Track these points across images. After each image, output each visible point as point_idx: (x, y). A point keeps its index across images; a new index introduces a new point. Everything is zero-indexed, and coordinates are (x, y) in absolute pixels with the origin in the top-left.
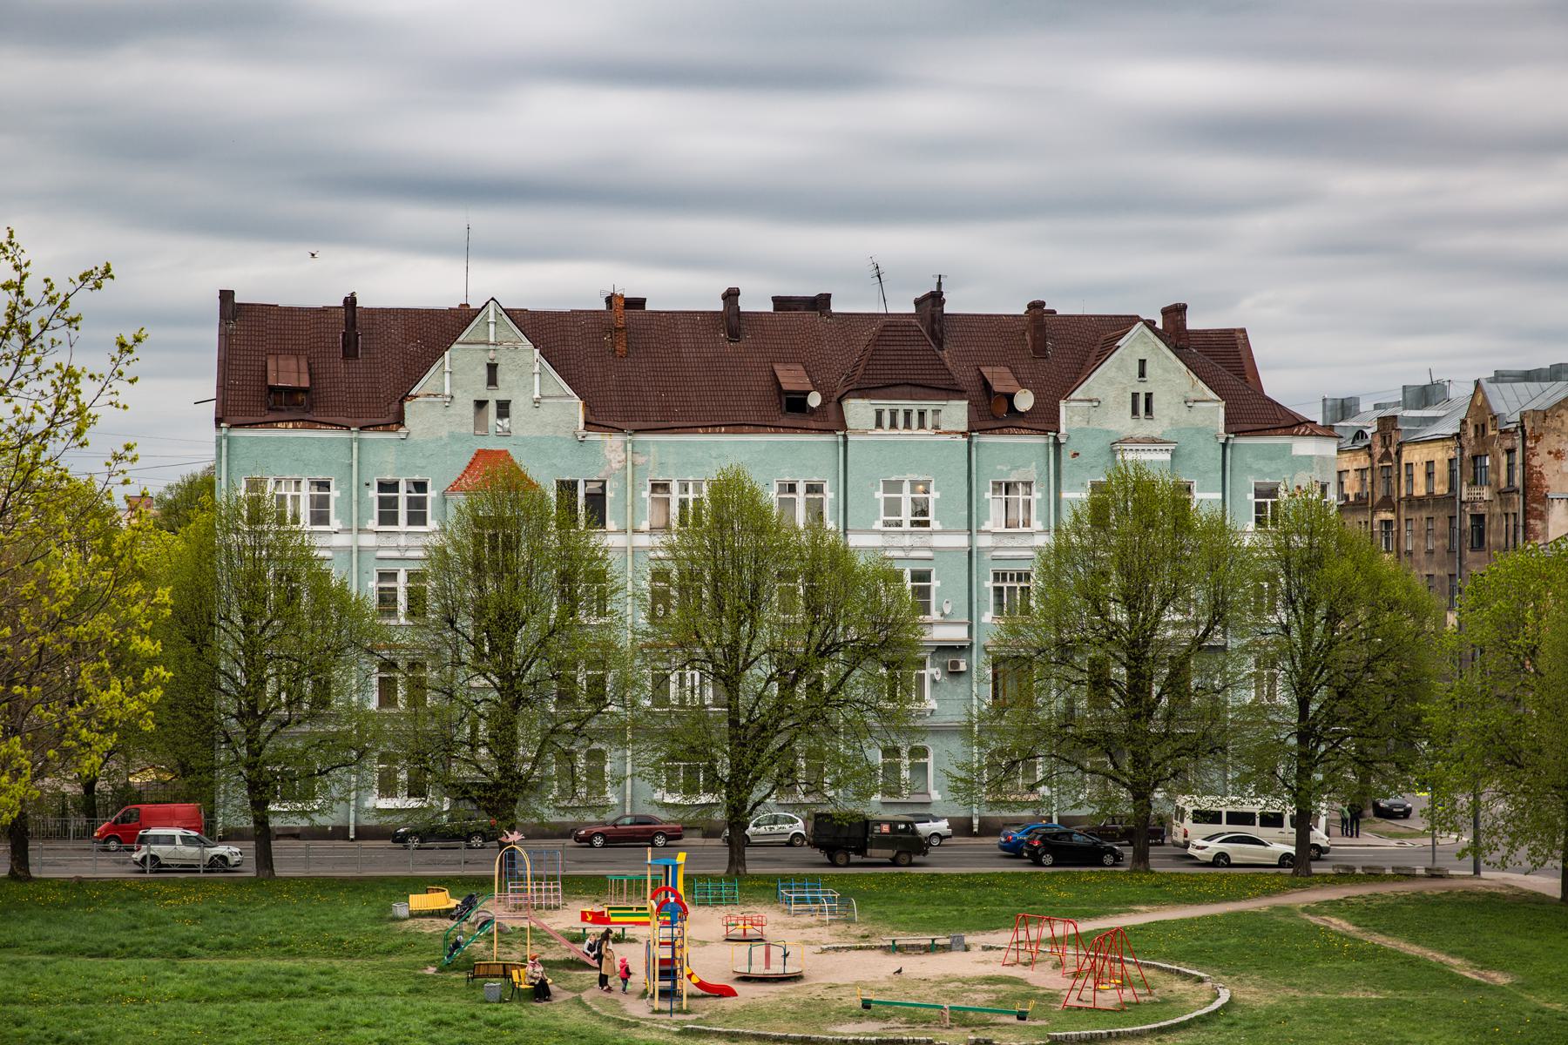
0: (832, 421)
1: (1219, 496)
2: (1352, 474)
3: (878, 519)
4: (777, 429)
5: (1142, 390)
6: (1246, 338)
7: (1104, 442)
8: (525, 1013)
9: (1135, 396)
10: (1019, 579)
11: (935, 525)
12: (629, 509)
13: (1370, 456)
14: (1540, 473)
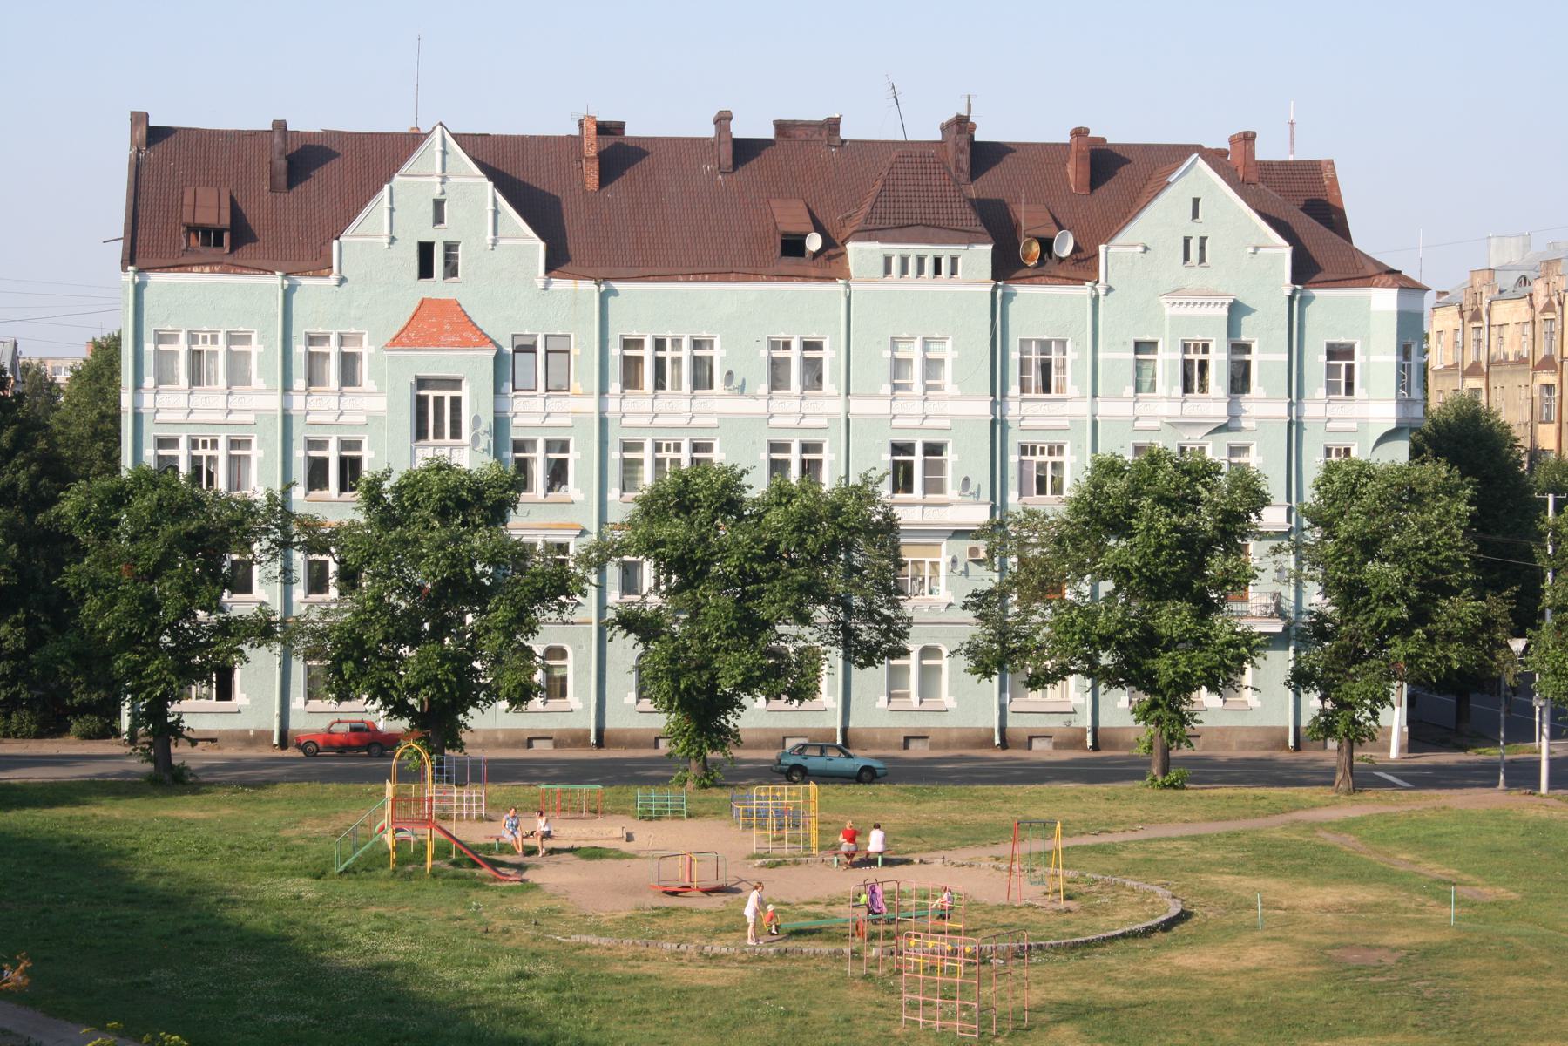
0: (830, 263)
2: (1512, 326)
4: (771, 277)
5: (1195, 233)
6: (1333, 170)
10: (1051, 453)
11: (950, 388)
13: (1532, 306)
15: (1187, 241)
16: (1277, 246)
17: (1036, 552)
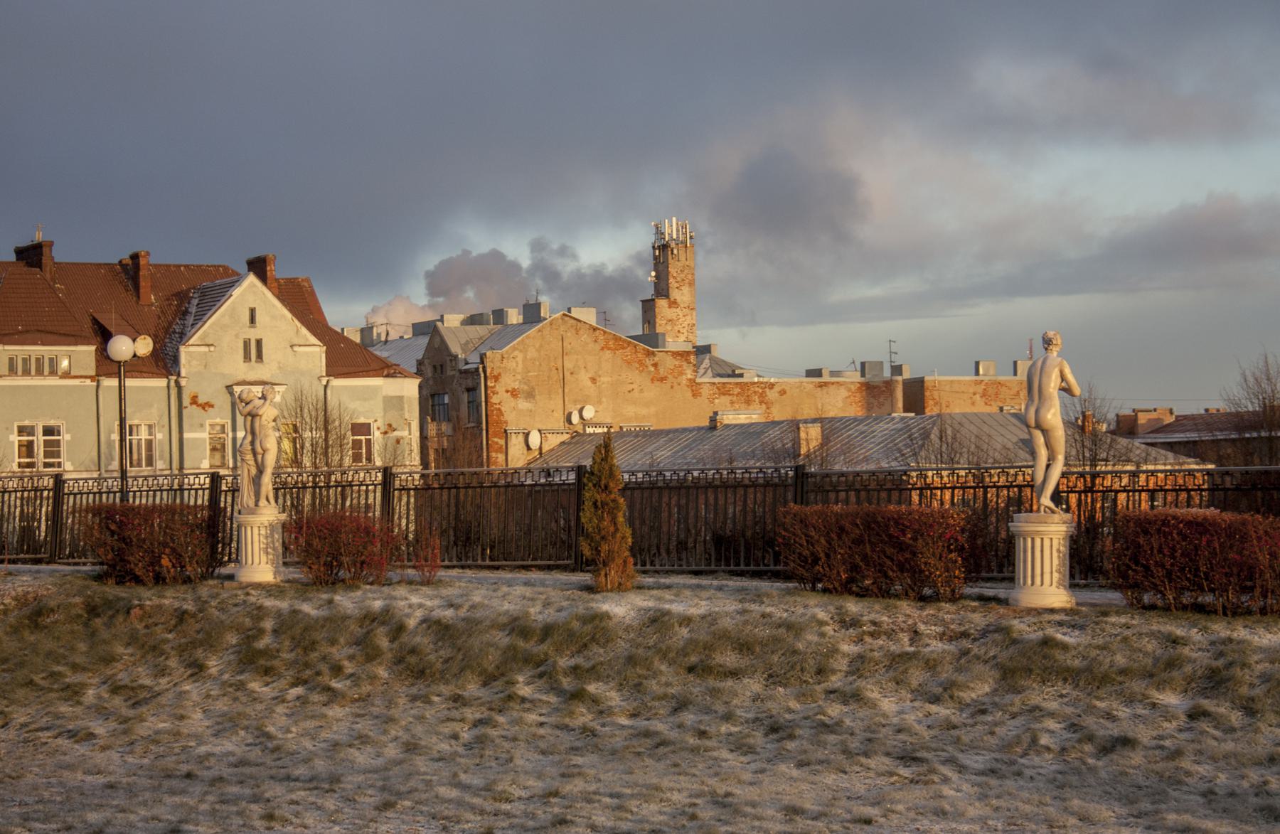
1: (186, 435)
3: (13, 461)
5: (253, 335)
7: (220, 386)
8: (332, 767)
9: (247, 344)
12: (484, 432)
14: (499, 409)
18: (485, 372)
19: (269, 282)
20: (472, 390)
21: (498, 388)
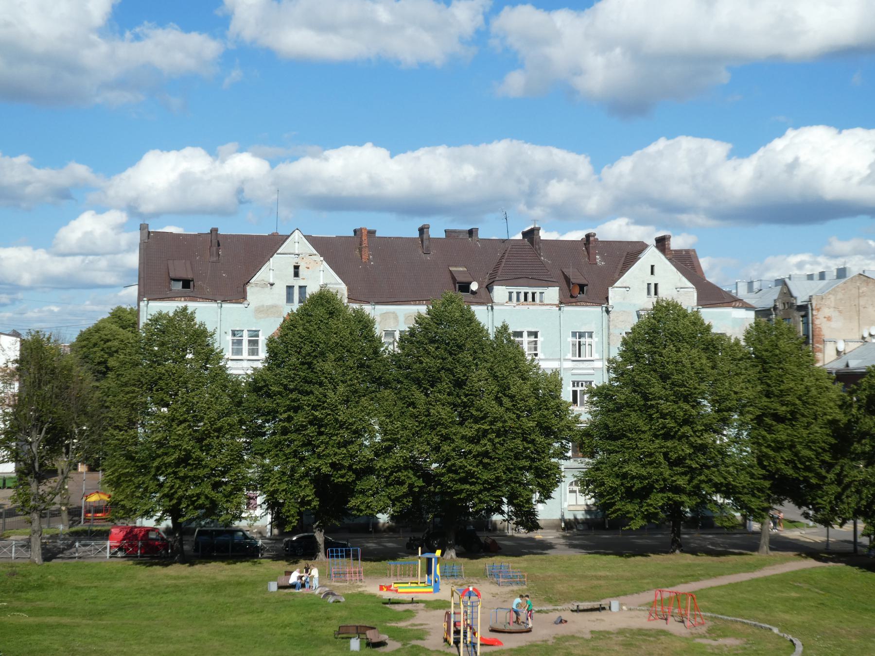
5: (653, 280)
15: (649, 284)
16: (340, 284)
17: (748, 449)
18: (812, 306)
19: (281, 232)
20: (805, 316)
21: (819, 316)
